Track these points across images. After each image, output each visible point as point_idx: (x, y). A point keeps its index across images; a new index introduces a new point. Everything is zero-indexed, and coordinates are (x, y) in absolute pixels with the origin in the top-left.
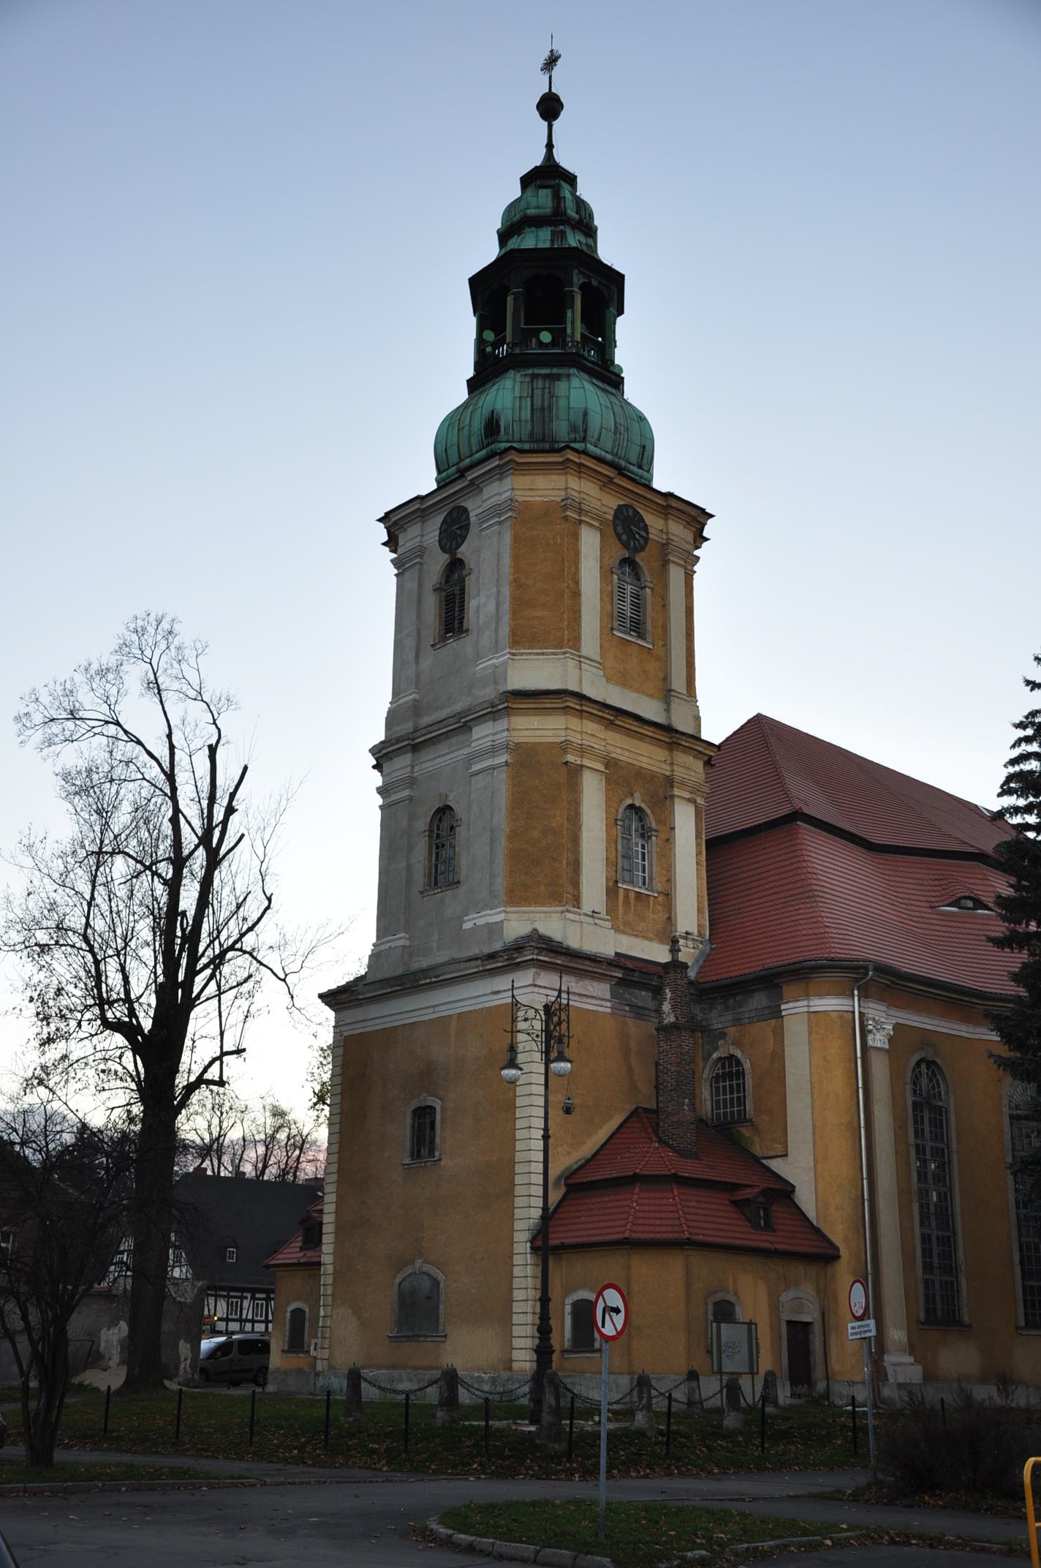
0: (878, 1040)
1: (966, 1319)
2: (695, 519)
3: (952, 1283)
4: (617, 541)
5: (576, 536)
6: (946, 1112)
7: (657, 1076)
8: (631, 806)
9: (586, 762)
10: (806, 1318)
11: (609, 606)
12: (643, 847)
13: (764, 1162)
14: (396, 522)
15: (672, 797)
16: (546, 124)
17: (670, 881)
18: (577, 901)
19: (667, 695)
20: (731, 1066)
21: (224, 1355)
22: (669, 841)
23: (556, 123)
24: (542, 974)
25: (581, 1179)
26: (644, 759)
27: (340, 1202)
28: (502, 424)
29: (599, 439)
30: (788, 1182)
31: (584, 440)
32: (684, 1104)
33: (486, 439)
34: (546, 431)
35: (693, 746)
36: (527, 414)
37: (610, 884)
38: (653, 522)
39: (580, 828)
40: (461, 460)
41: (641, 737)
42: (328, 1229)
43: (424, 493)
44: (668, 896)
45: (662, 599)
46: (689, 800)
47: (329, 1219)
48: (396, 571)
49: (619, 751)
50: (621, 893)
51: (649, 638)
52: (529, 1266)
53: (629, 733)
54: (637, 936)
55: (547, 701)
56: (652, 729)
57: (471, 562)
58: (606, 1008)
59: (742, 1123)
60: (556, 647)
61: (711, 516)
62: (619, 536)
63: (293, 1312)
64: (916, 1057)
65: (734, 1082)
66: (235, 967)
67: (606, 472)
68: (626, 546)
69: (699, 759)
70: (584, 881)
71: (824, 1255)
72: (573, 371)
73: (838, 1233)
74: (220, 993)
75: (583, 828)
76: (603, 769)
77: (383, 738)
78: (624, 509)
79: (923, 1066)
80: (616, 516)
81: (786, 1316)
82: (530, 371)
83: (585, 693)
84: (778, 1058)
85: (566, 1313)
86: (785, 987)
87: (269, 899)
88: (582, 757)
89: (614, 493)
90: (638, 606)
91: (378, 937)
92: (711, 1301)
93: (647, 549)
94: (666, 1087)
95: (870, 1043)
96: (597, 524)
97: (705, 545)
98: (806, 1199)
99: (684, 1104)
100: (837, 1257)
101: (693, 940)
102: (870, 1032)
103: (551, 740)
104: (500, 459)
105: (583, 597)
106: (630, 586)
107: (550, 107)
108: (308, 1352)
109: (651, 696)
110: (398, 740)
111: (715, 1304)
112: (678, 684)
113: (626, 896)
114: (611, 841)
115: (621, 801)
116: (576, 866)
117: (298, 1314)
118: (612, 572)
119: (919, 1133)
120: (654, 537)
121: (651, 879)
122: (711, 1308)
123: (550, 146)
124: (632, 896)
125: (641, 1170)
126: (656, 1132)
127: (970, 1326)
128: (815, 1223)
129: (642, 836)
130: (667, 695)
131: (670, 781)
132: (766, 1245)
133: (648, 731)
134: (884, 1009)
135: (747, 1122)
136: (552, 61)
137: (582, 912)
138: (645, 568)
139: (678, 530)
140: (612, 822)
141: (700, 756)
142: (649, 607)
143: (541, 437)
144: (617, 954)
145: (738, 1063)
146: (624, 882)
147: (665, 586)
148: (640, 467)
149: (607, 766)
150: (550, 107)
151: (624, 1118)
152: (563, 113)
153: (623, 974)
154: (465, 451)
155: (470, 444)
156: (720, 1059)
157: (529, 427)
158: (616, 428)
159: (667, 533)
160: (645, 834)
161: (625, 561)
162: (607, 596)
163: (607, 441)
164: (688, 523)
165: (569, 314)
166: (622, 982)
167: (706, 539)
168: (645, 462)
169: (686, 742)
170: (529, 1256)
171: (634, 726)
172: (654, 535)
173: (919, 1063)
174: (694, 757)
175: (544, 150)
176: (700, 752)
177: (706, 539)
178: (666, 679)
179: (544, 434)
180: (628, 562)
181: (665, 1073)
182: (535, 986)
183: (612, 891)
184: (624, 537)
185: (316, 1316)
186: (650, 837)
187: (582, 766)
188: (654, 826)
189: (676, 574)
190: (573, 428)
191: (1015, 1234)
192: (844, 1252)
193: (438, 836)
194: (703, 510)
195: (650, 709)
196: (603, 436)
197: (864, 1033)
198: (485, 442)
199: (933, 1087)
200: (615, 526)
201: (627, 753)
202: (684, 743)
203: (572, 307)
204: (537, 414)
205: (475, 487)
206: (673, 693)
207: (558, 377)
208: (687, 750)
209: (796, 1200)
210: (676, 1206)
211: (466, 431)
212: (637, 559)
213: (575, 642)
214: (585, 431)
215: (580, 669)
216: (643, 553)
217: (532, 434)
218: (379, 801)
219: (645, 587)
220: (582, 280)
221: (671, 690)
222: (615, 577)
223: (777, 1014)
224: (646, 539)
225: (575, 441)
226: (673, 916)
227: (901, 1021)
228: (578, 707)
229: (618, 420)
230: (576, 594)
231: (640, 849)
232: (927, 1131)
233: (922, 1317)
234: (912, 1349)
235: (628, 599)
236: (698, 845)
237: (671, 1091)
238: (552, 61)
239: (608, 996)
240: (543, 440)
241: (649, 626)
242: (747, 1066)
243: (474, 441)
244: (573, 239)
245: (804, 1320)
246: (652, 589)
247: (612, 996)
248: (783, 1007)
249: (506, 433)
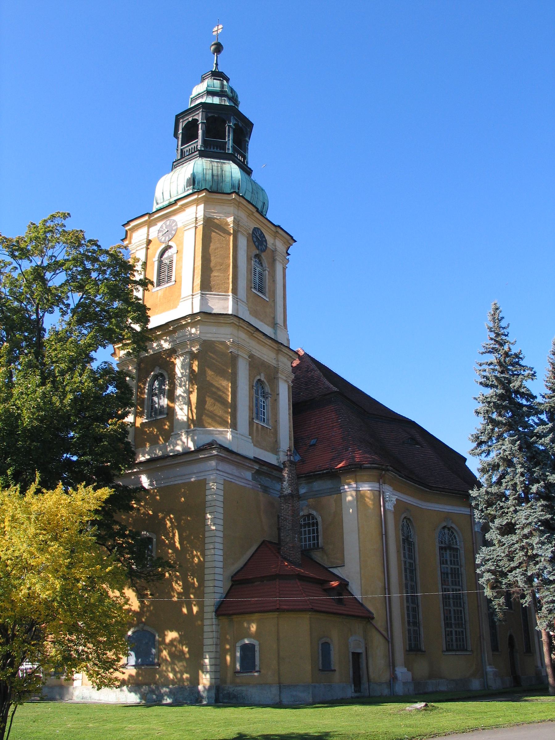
1: (423, 648)
2: (288, 241)
3: (462, 632)
4: (254, 245)
6: (414, 544)
7: (278, 522)
11: (250, 276)
13: (331, 570)
17: (276, 421)
19: (274, 325)
20: (309, 520)
22: (276, 401)
24: (220, 464)
26: (266, 357)
30: (344, 580)
32: (295, 537)
33: (187, 187)
34: (219, 187)
35: (288, 353)
37: (250, 420)
39: (237, 387)
45: (273, 277)
50: (255, 425)
51: (267, 295)
52: (214, 626)
55: (221, 319)
56: (270, 341)
59: (316, 549)
61: (295, 241)
64: (403, 516)
65: (311, 528)
67: (251, 209)
68: (257, 248)
69: (289, 360)
70: (239, 415)
71: (368, 618)
76: (247, 358)
78: (257, 230)
85: (258, 652)
86: (342, 478)
89: (253, 221)
92: (320, 643)
94: (285, 528)
99: (295, 537)
106: (258, 269)
109: (268, 325)
112: (280, 320)
113: (257, 427)
114: (251, 398)
115: (255, 377)
120: (270, 247)
124: (260, 427)
125: (279, 572)
126: (279, 553)
127: (425, 651)
128: (361, 601)
129: (264, 397)
130: (274, 325)
135: (319, 549)
137: (238, 432)
138: (265, 260)
139: (280, 246)
140: (251, 387)
141: (290, 359)
142: (267, 281)
143: (216, 189)
144: (254, 457)
145: (313, 518)
146: (257, 418)
149: (249, 357)
153: (259, 468)
156: (304, 516)
161: (257, 256)
162: (249, 270)
164: (284, 243)
168: (264, 210)
169: (285, 350)
170: (214, 620)
171: (262, 338)
174: (288, 359)
176: (290, 357)
179: (218, 188)
180: (257, 256)
181: (285, 521)
182: (218, 470)
184: (257, 244)
186: (267, 398)
189: (279, 267)
190: (233, 186)
191: (442, 606)
195: (268, 330)
196: (247, 193)
198: (186, 189)
201: (258, 352)
202: (284, 351)
206: (278, 325)
207: (224, 163)
209: (349, 589)
210: (300, 591)
215: (237, 304)
217: (211, 187)
219: (265, 270)
220: (235, 122)
224: (266, 247)
226: (278, 440)
227: (399, 498)
228: (237, 324)
229: (253, 188)
233: (408, 649)
235: (257, 275)
236: (289, 405)
237: (289, 530)
241: (267, 290)
242: (319, 520)
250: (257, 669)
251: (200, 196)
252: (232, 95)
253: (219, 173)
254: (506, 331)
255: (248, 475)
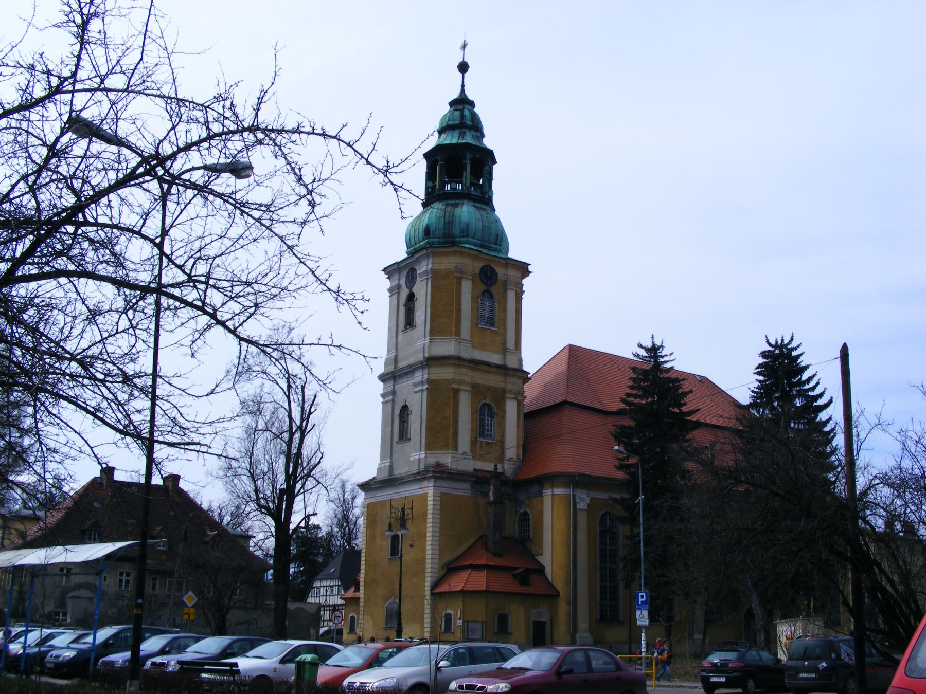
0: (582, 505)
1: (621, 619)
5: (459, 285)
8: (485, 404)
9: (462, 387)
10: (543, 620)
12: (491, 421)
14: (390, 271)
15: (505, 398)
16: (461, 74)
17: (503, 435)
18: (456, 448)
19: (504, 351)
21: (327, 635)
22: (503, 418)
23: (465, 75)
25: (453, 565)
27: (366, 573)
28: (431, 230)
29: (474, 235)
31: (467, 236)
36: (442, 225)
38: (500, 271)
40: (416, 244)
41: (490, 372)
42: (362, 584)
43: (399, 260)
44: (502, 442)
46: (513, 398)
47: (362, 580)
48: (389, 294)
49: (479, 380)
50: (479, 443)
51: (496, 325)
53: (483, 371)
54: (486, 461)
57: (417, 295)
58: (469, 494)
60: (449, 335)
61: (530, 265)
62: (482, 280)
63: (351, 617)
64: (603, 512)
66: (310, 483)
68: (485, 284)
71: (552, 596)
72: (465, 201)
73: (559, 585)
74: (304, 492)
75: (460, 416)
77: (383, 371)
79: (608, 516)
80: (481, 271)
81: (533, 619)
82: (446, 202)
83: (462, 356)
84: (541, 513)
87: (322, 454)
88: (460, 385)
90: (492, 311)
91: (381, 460)
93: (497, 284)
95: (578, 507)
96: (470, 277)
97: (531, 274)
98: (548, 572)
100: (558, 595)
101: (514, 461)
102: (578, 502)
103: (446, 378)
104: (427, 250)
105: (462, 312)
107: (463, 67)
108: (356, 633)
110: (388, 374)
111: (499, 615)
112: (511, 344)
116: (456, 433)
117: (352, 618)
118: (478, 298)
119: (602, 543)
121: (494, 435)
122: (496, 616)
123: (463, 86)
124: (484, 443)
131: (504, 391)
132: (524, 591)
133: (494, 370)
134: (586, 492)
136: (464, 46)
140: (474, 412)
144: (475, 470)
147: (505, 301)
148: (496, 244)
150: (463, 67)
151: (474, 541)
152: (469, 69)
154: (417, 240)
155: (419, 238)
157: (443, 231)
158: (483, 228)
159: (507, 275)
160: (492, 415)
161: (484, 292)
163: (479, 235)
165: (464, 173)
166: (476, 483)
167: (531, 272)
168: (498, 241)
171: (486, 368)
172: (500, 277)
173: (605, 513)
175: (460, 88)
177: (531, 272)
178: (504, 344)
183: (474, 443)
184: (485, 280)
185: (358, 619)
187: (459, 389)
188: (496, 411)
189: (511, 295)
190: (462, 231)
192: (562, 594)
193: (404, 417)
194: (525, 263)
195: (495, 358)
197: (575, 503)
199: (613, 524)
200: (480, 277)
201: (483, 380)
203: (466, 170)
204: (446, 225)
205: (418, 261)
208: (513, 376)
211: (417, 232)
212: (491, 290)
213: (458, 333)
214: (467, 232)
216: (494, 287)
217: (444, 235)
218: (381, 400)
220: (471, 156)
221: (506, 349)
222: (480, 300)
223: (541, 495)
225: (463, 237)
230: (459, 311)
231: (489, 422)
232: (608, 541)
233: (598, 619)
234: (591, 631)
236: (518, 418)
238: (464, 46)
239: (469, 488)
240: (449, 237)
241: (496, 320)
243: (421, 236)
244: (468, 139)
245: (542, 620)
246: (498, 303)
247: (472, 488)
248: (543, 492)
249: (433, 235)
250: (452, 631)
251: (428, 251)
252: (471, 123)
253: (451, 220)
254: (672, 358)
255: (467, 486)
